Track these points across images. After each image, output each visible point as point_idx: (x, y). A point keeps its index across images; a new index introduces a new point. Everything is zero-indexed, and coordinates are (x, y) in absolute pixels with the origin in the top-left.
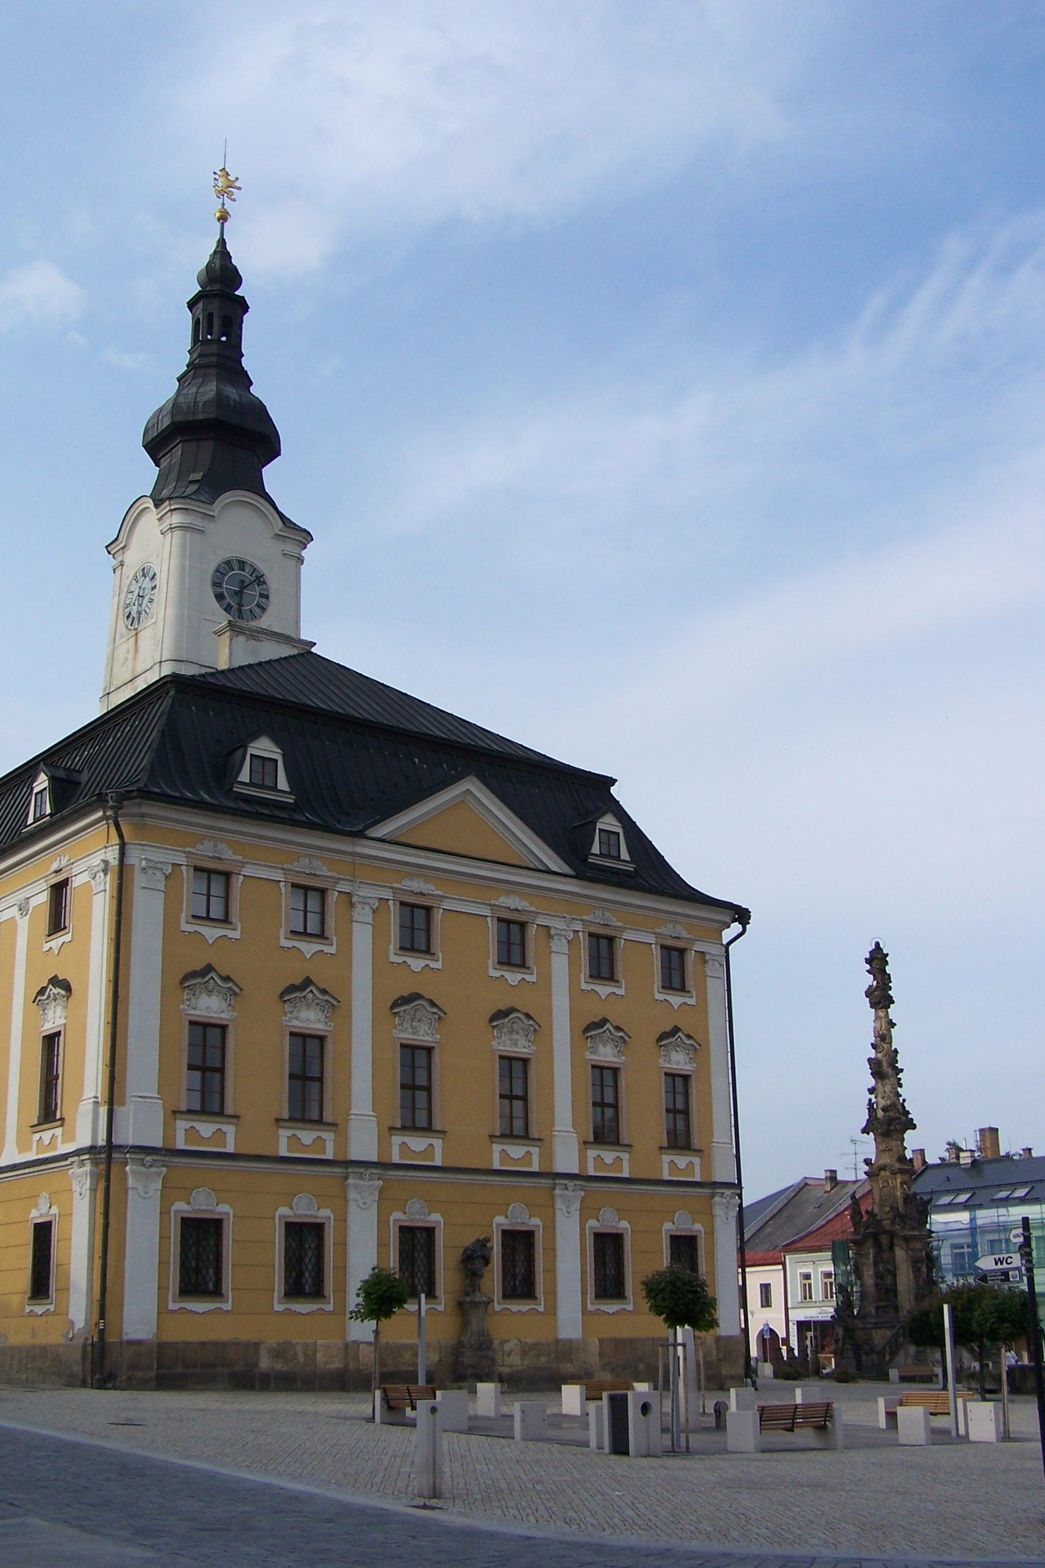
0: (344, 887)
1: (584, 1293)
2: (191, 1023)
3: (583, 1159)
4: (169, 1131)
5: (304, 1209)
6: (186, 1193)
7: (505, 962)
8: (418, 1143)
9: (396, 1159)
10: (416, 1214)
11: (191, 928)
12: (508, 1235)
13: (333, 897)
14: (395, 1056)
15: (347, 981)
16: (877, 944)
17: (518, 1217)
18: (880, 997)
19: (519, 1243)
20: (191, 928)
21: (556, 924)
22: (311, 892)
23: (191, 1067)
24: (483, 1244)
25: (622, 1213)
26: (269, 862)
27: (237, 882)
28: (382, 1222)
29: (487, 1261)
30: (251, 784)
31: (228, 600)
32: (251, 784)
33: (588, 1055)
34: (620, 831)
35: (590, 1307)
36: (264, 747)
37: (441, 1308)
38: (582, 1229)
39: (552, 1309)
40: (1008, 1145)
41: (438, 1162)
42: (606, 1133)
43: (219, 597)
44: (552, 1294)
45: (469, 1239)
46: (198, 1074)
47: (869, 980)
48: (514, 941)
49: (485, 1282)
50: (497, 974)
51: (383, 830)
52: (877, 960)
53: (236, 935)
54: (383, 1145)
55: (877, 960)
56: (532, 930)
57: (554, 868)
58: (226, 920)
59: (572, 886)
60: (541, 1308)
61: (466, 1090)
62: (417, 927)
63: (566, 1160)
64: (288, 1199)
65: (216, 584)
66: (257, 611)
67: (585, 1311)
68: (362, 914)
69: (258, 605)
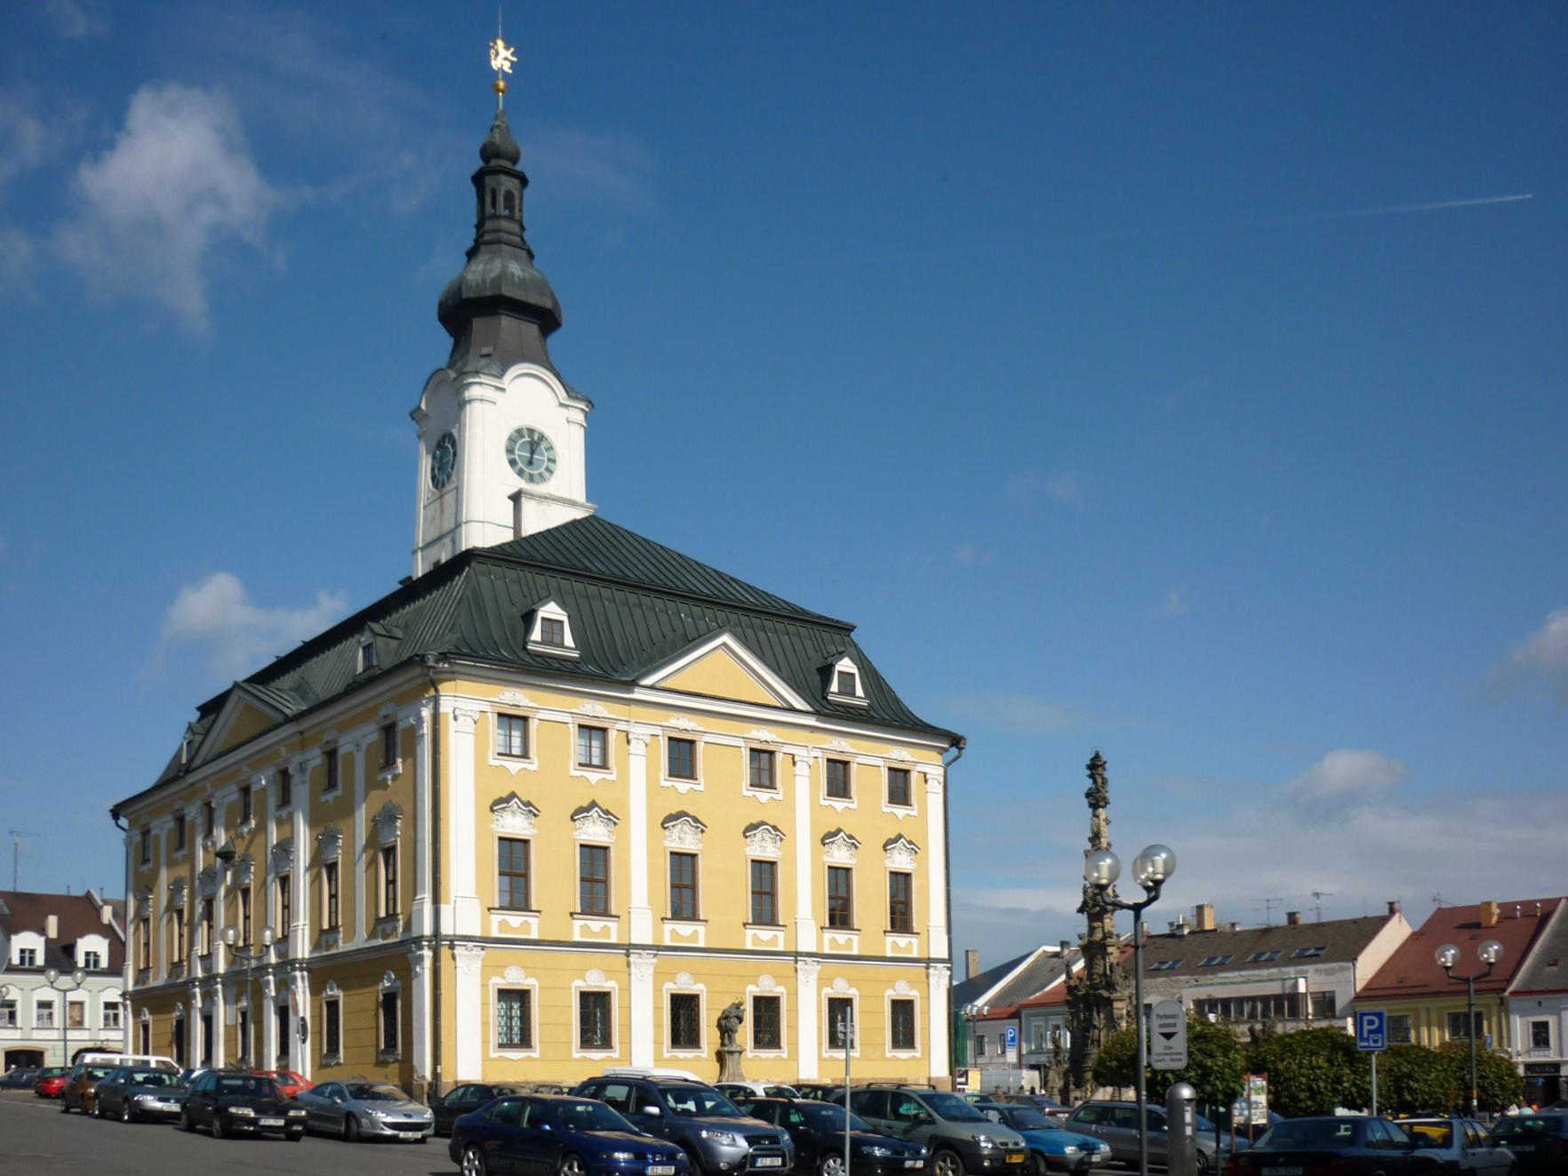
0: (623, 726)
1: (820, 1044)
2: (501, 839)
3: (820, 941)
4: (485, 924)
5: (595, 981)
6: (672, 977)
7: (756, 783)
8: (685, 929)
9: (667, 942)
10: (685, 985)
11: (497, 763)
12: (758, 1000)
13: (612, 735)
14: (666, 864)
15: (625, 804)
16: (1097, 756)
17: (767, 987)
18: (1096, 799)
19: (767, 1009)
20: (497, 763)
21: (800, 753)
22: (593, 731)
23: (501, 874)
24: (738, 1006)
25: (697, 977)
26: (556, 711)
27: (533, 725)
28: (657, 991)
29: (741, 1020)
30: (542, 643)
31: (520, 465)
32: (542, 643)
33: (825, 858)
34: (565, 619)
35: (825, 1055)
36: (551, 610)
37: (704, 1055)
38: (819, 995)
39: (794, 1056)
40: (1304, 919)
41: (701, 944)
42: (840, 916)
43: (513, 463)
44: (794, 1044)
45: (726, 1003)
46: (507, 879)
47: (1089, 783)
48: (763, 766)
49: (738, 1037)
50: (750, 794)
51: (648, 681)
52: (1095, 766)
53: (534, 767)
54: (657, 932)
55: (1095, 766)
56: (779, 757)
57: (798, 706)
58: (525, 755)
59: (811, 721)
60: (785, 1055)
61: (723, 889)
62: (682, 757)
63: (807, 942)
64: (581, 973)
65: (510, 451)
66: (546, 474)
67: (820, 1059)
68: (637, 747)
69: (547, 469)
